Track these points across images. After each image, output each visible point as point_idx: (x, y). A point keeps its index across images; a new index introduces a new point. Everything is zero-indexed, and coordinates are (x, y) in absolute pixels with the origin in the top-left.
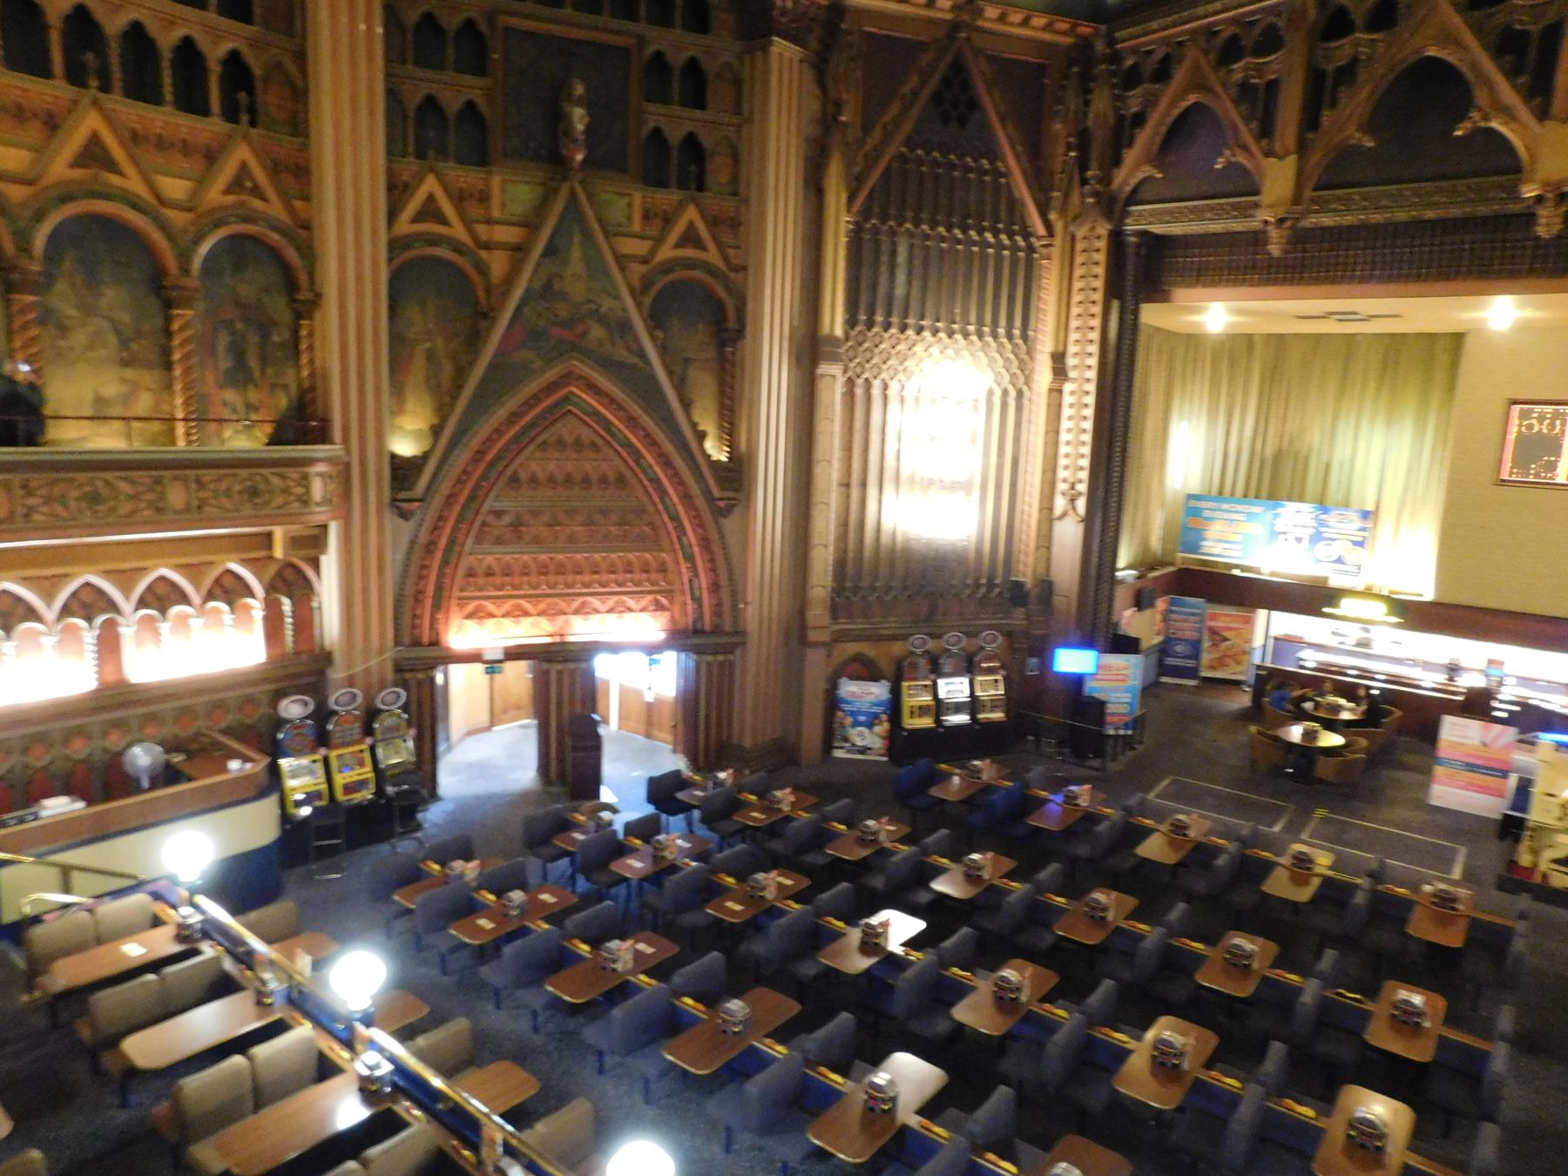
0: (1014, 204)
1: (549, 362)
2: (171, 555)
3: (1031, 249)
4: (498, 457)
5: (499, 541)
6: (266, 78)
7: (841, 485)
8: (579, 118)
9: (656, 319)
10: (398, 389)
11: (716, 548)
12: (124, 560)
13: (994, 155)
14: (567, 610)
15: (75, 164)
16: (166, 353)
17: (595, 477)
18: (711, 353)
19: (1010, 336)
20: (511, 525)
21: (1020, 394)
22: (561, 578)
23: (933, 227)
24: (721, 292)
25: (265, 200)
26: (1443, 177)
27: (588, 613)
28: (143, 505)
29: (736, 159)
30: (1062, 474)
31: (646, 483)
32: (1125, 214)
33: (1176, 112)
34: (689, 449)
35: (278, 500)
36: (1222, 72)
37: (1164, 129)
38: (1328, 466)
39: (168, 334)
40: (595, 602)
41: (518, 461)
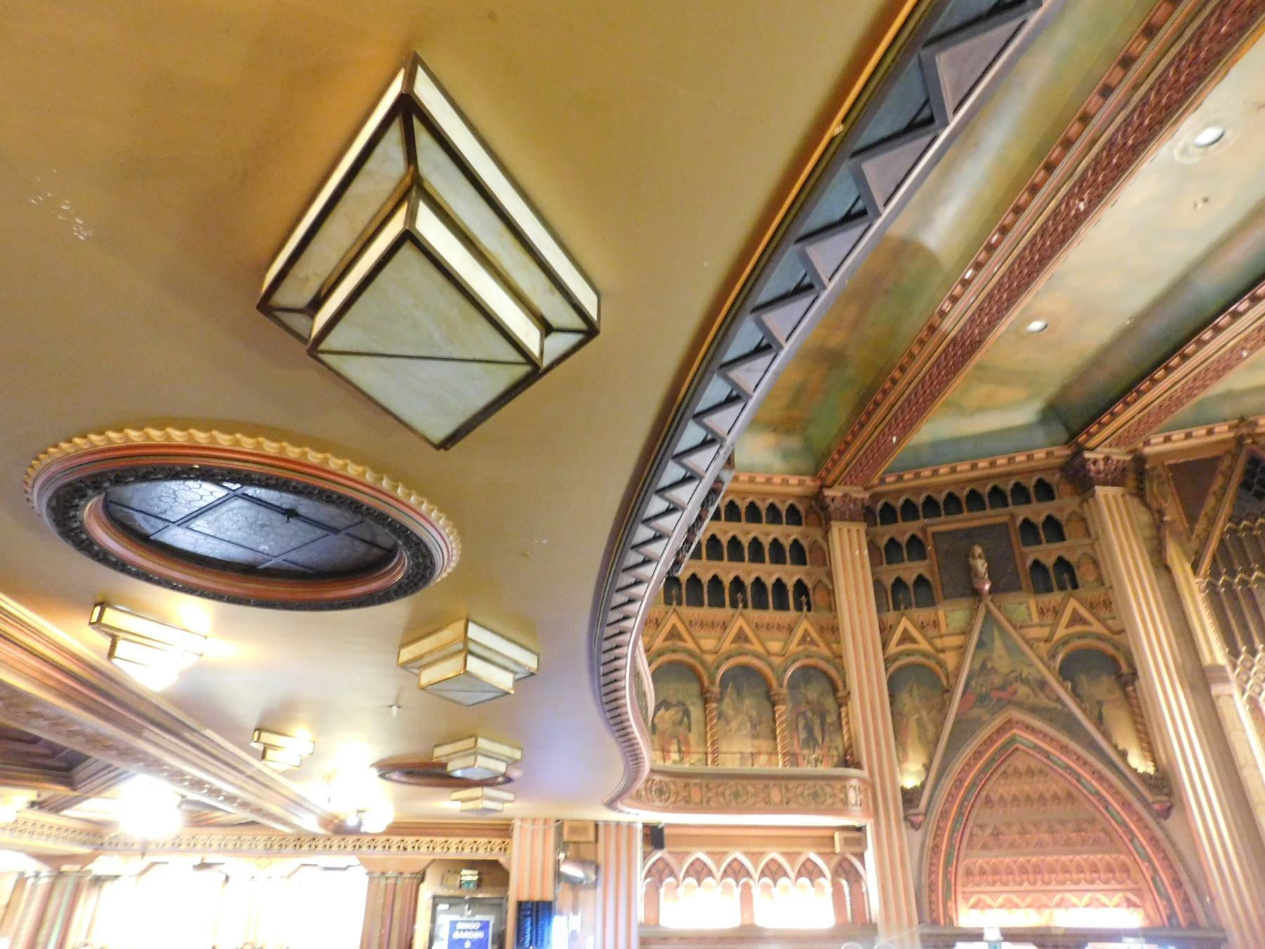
1: (994, 714)
4: (974, 783)
5: (985, 847)
8: (981, 565)
9: (1066, 673)
11: (1166, 844)
16: (774, 731)
18: (1118, 694)
29: (1096, 563)
31: (1090, 796)
35: (829, 801)
39: (774, 720)
40: (1072, 898)
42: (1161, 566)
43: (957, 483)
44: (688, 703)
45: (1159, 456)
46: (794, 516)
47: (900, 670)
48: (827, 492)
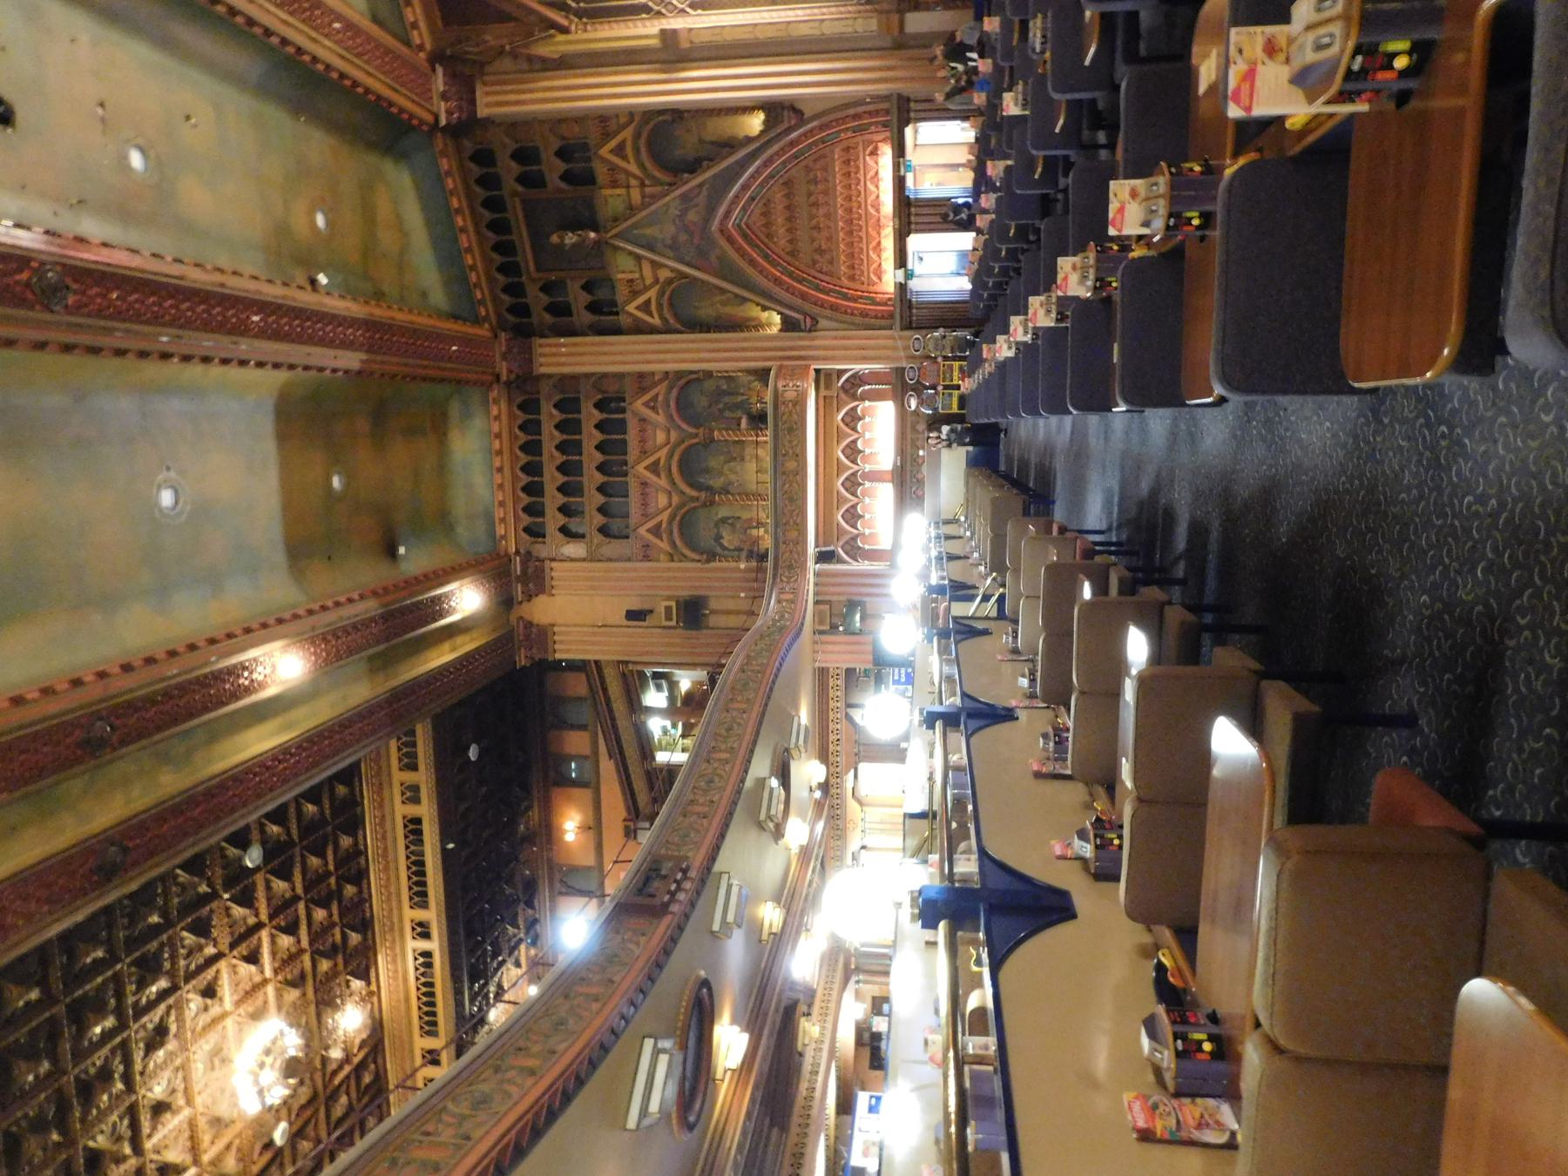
5: (831, 262)
6: (600, 391)
16: (737, 442)
42: (564, 64)
43: (480, 244)
44: (716, 518)
45: (433, 32)
46: (530, 406)
47: (676, 316)
48: (504, 378)
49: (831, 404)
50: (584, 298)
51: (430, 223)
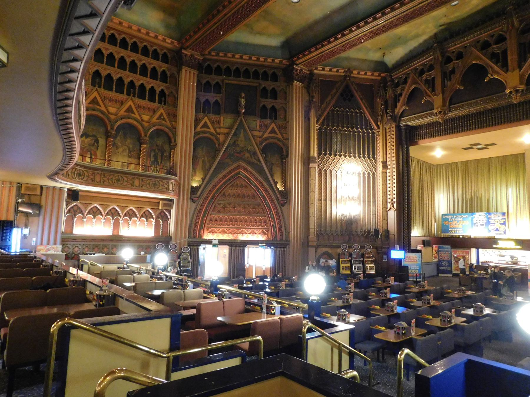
0: (367, 122)
2: (133, 204)
3: (373, 133)
4: (220, 188)
5: (219, 211)
6: (169, 95)
7: (319, 200)
8: (243, 102)
9: (264, 151)
10: (194, 169)
12: (123, 203)
13: (360, 108)
14: (247, 232)
15: (125, 111)
16: (139, 155)
17: (246, 195)
19: (369, 158)
20: (223, 207)
21: (374, 174)
22: (236, 223)
23: (343, 127)
24: (282, 145)
25: (166, 121)
26: (489, 95)
27: (243, 234)
28: (129, 184)
29: (285, 112)
30: (389, 197)
32: (400, 121)
33: (410, 91)
34: (272, 187)
36: (420, 78)
37: (407, 96)
38: (488, 201)
39: (140, 151)
41: (225, 190)
42: (307, 119)
43: (241, 64)
46: (165, 59)
49: (155, 206)
50: (212, 100)
51: (247, 45)
